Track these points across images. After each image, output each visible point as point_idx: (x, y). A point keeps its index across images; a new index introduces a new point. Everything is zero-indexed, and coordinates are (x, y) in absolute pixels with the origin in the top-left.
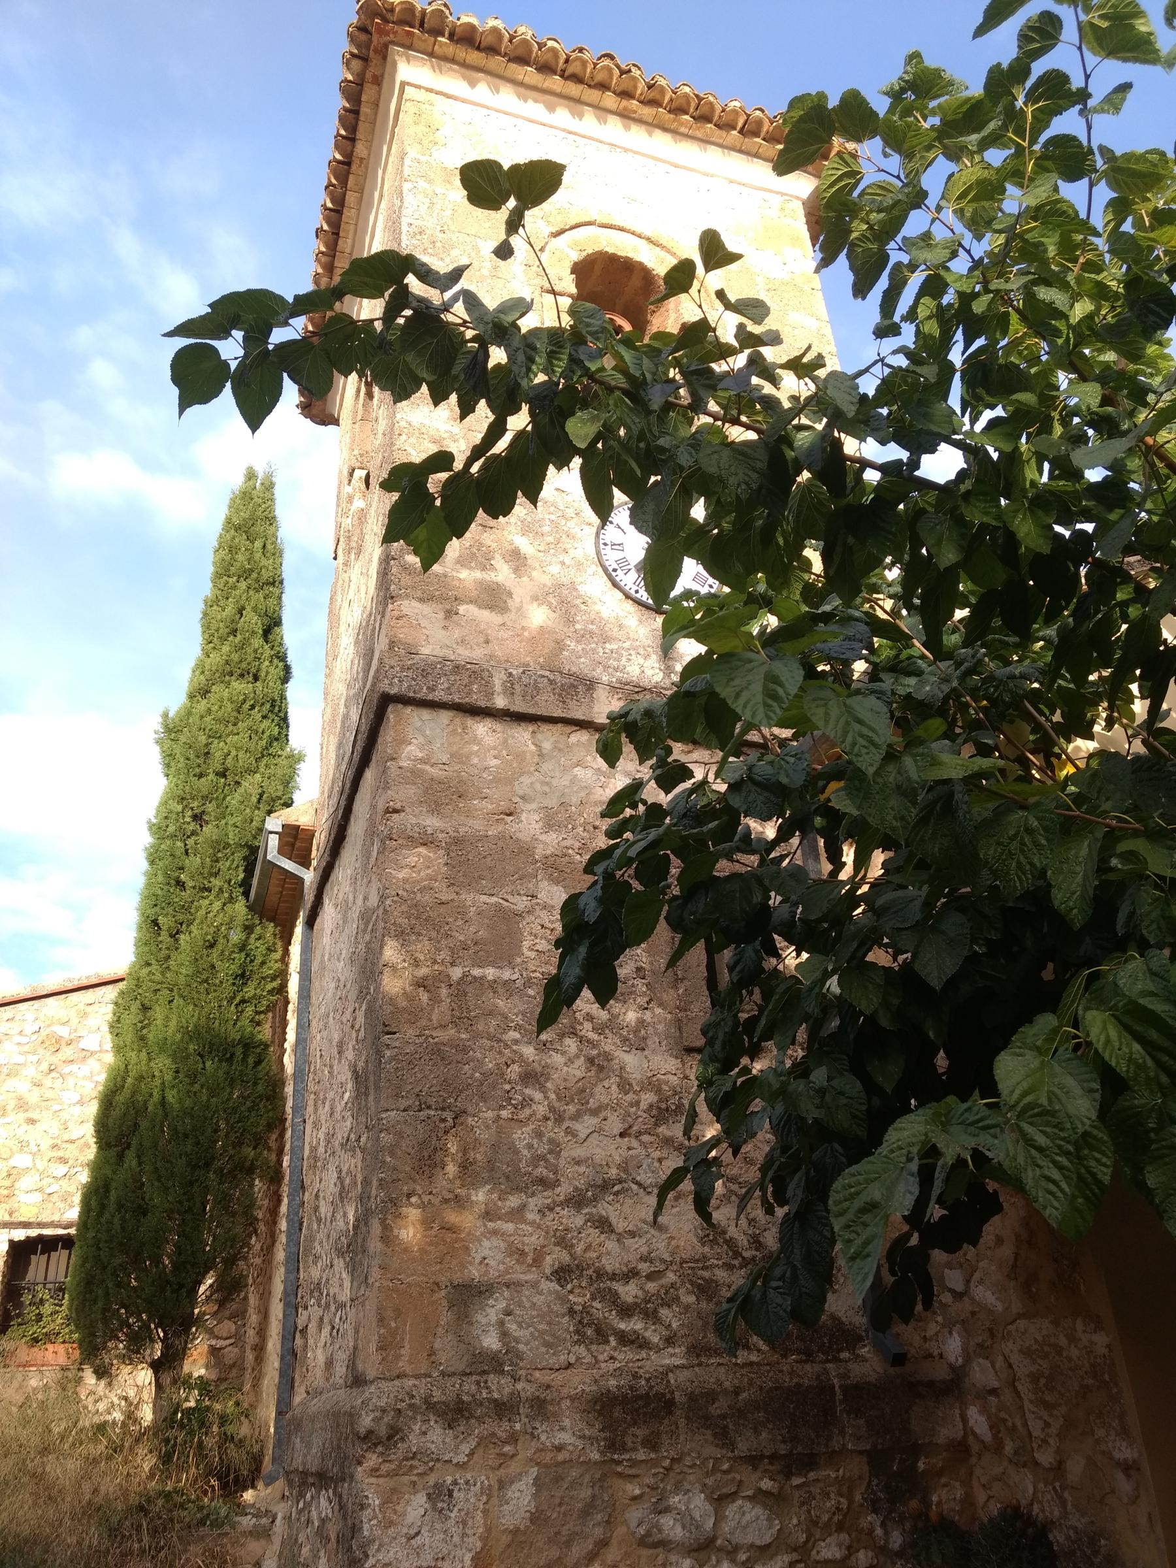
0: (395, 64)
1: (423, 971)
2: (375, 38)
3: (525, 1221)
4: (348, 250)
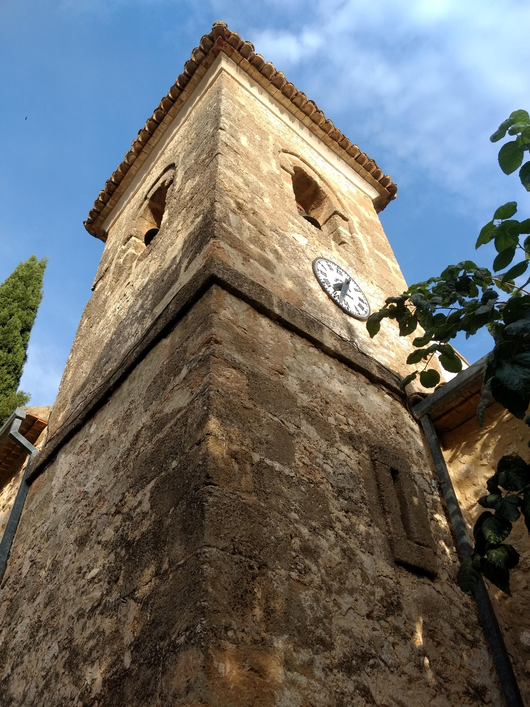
1: (235, 447)
2: (216, 44)
3: (313, 677)
4: (153, 145)
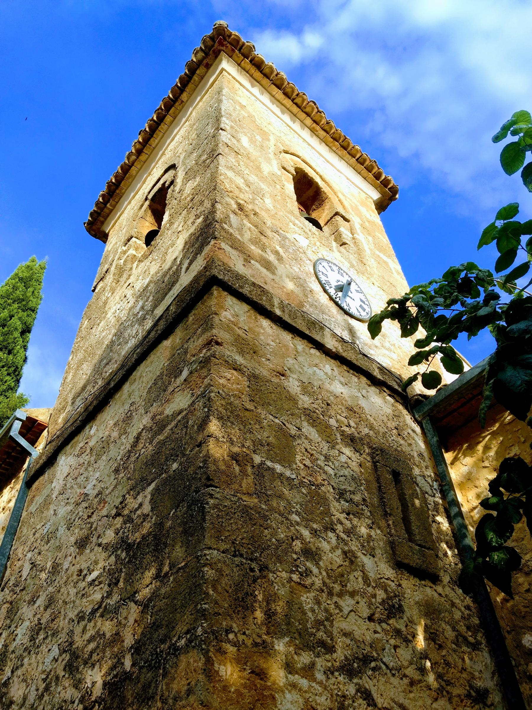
0: (221, 60)
2: (216, 45)
4: (154, 146)
